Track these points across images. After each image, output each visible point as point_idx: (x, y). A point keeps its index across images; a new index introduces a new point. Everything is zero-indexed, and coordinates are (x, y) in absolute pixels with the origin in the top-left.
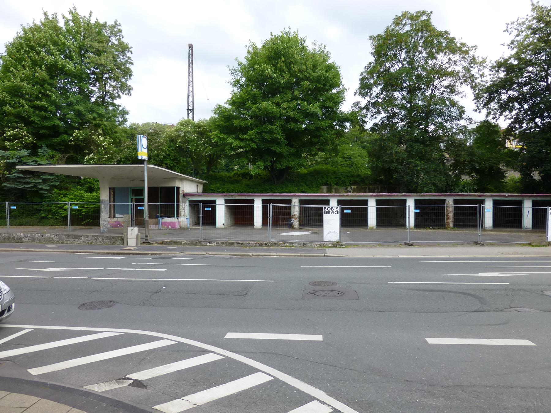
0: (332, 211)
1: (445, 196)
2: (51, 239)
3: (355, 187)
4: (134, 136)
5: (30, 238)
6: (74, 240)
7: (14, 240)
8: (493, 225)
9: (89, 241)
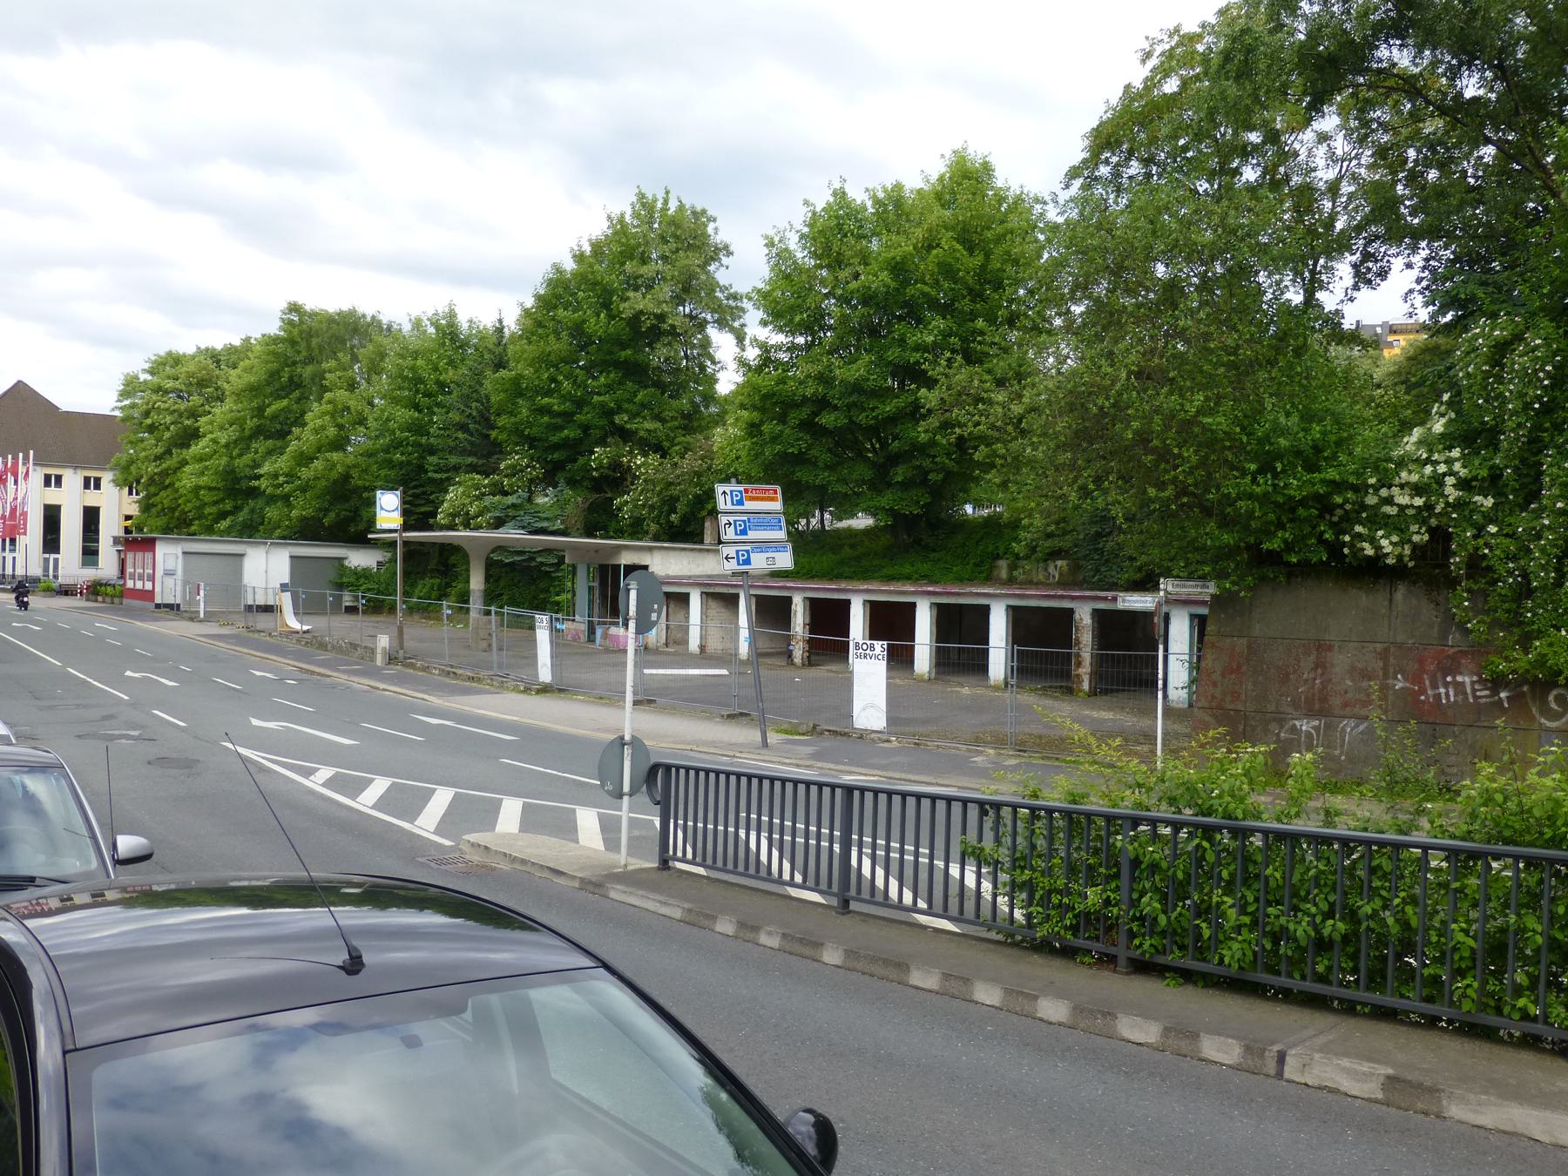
1: (1073, 598)
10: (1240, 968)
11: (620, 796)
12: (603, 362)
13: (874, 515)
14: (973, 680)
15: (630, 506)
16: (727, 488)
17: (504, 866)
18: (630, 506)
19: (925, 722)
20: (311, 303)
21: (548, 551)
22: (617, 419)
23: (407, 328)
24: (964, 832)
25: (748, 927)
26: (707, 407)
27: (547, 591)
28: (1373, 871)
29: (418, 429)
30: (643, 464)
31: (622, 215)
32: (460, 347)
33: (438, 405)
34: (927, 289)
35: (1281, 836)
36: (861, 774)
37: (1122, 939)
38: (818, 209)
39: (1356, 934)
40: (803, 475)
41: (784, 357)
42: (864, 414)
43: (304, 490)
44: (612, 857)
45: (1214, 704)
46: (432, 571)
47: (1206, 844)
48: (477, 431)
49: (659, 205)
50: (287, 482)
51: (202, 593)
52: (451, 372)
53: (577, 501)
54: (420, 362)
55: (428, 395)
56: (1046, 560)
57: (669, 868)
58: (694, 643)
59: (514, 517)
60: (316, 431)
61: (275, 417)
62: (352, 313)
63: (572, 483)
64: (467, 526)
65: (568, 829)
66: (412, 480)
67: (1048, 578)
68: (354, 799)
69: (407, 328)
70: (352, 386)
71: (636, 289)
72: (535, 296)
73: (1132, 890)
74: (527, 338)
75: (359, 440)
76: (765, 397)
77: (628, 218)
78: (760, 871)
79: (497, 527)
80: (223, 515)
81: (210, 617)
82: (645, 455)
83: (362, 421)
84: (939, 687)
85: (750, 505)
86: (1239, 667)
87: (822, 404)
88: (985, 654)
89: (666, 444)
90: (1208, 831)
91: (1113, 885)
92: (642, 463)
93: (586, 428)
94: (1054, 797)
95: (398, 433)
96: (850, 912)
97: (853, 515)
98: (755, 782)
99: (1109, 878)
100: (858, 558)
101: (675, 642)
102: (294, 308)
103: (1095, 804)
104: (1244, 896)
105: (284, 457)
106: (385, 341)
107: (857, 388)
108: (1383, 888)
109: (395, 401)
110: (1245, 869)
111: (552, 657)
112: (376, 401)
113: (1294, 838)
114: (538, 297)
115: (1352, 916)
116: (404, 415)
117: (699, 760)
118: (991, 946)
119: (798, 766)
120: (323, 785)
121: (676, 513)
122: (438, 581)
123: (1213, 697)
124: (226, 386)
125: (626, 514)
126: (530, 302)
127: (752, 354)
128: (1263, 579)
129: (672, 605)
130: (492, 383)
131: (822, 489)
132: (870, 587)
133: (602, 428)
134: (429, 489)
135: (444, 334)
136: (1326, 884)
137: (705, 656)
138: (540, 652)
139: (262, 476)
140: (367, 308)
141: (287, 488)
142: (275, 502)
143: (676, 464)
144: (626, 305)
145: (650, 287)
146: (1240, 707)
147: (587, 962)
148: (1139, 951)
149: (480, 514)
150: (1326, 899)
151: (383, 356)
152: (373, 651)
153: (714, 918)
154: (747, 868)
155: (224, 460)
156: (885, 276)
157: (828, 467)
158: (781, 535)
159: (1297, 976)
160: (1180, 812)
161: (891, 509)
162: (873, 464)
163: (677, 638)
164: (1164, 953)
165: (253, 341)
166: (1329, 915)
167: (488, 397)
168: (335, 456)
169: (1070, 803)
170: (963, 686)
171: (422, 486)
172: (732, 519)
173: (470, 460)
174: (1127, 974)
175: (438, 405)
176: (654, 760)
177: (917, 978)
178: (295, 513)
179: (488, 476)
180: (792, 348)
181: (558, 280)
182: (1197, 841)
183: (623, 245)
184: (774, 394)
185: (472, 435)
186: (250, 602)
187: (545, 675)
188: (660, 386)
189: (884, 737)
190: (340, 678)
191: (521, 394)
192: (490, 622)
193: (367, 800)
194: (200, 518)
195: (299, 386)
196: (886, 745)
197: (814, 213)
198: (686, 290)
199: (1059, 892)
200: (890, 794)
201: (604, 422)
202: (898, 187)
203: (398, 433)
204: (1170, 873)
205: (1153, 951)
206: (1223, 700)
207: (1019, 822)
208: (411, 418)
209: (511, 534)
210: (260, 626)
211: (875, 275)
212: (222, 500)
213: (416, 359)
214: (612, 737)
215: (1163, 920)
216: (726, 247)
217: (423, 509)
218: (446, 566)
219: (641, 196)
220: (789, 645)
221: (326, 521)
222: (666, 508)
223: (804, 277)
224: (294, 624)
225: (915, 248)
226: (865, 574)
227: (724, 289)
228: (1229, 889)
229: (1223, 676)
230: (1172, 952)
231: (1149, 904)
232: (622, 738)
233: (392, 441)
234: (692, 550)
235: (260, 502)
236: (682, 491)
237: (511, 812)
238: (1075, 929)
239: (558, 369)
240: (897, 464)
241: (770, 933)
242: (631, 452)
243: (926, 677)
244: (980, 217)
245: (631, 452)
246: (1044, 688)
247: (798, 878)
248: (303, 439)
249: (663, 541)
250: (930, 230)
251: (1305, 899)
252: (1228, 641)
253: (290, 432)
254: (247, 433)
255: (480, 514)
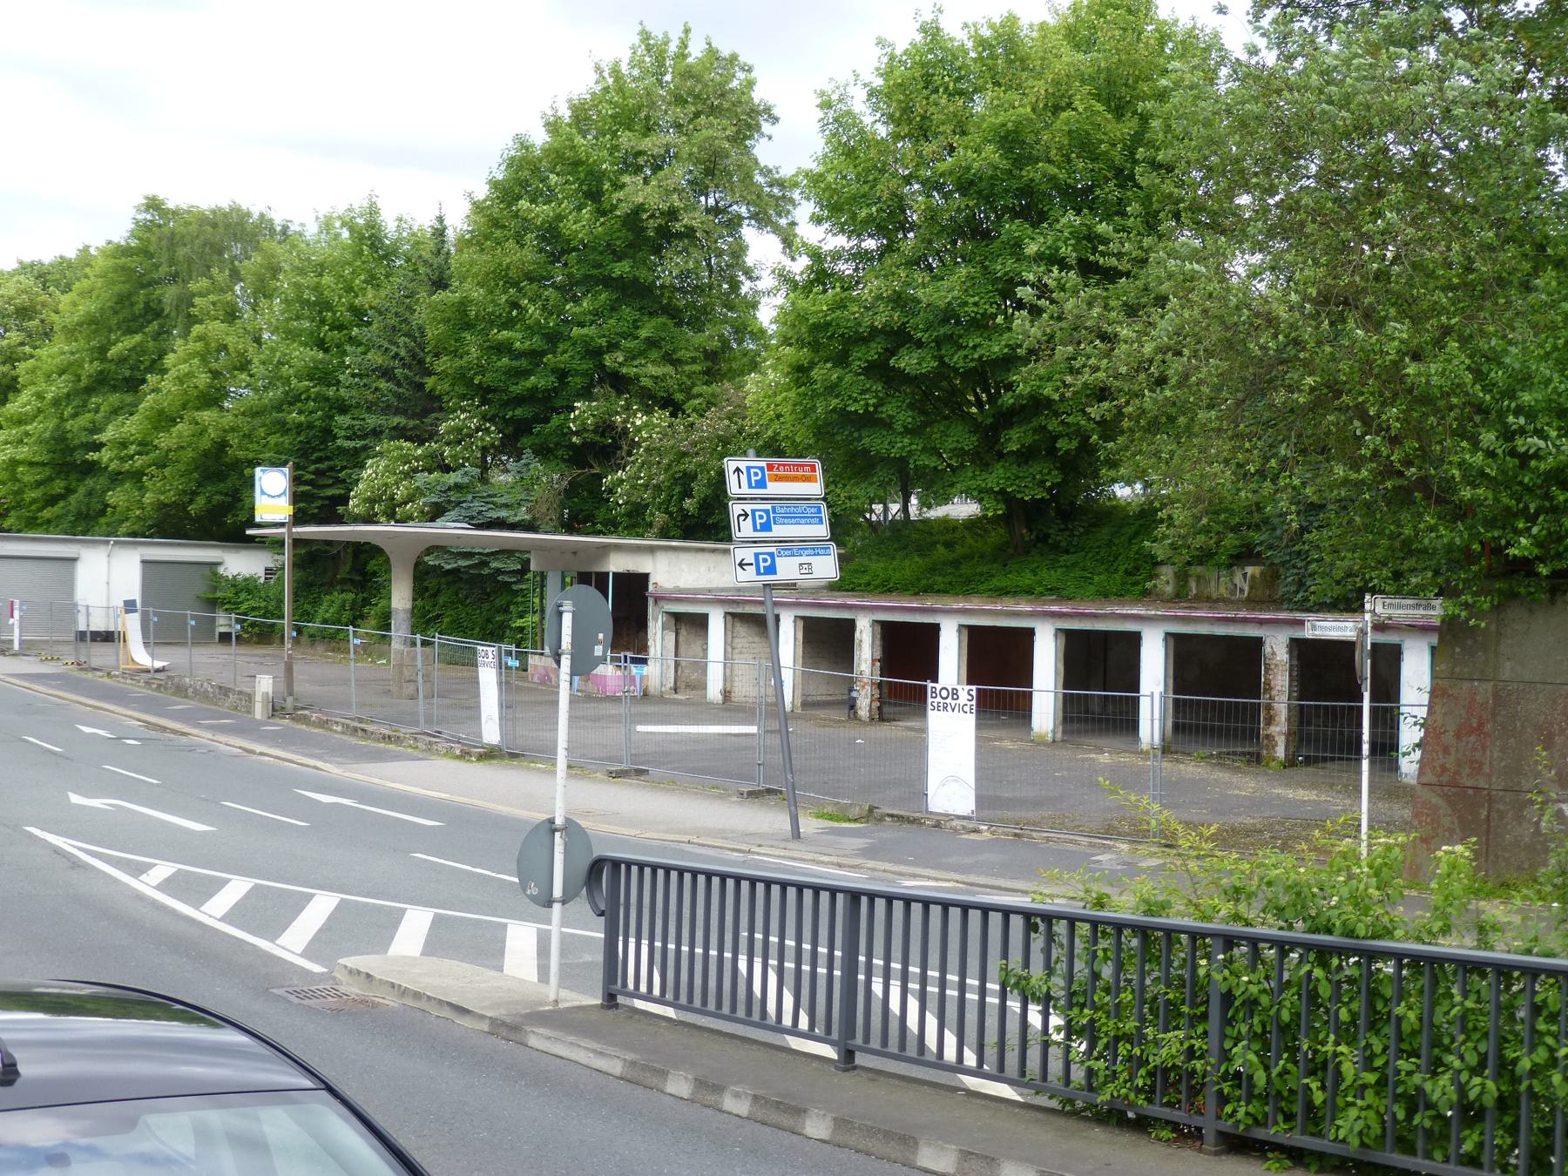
0: (953, 702)
1: (1262, 622)
10: (1363, 1144)
11: (549, 903)
12: (587, 278)
13: (980, 501)
14: (1117, 742)
15: (626, 486)
16: (743, 465)
17: (391, 1001)
18: (626, 486)
19: (1037, 804)
20: (175, 199)
21: (507, 553)
22: (608, 360)
23: (312, 230)
24: (1005, 955)
25: (708, 1087)
26: (740, 342)
27: (506, 610)
28: (1536, 1010)
29: (323, 376)
30: (645, 425)
31: (617, 63)
32: (385, 257)
33: (352, 340)
34: (1052, 170)
35: (1417, 960)
36: (929, 878)
37: (1211, 1104)
38: (898, 52)
39: (1516, 1096)
40: (874, 442)
41: (845, 268)
42: (962, 353)
43: (161, 465)
44: (543, 988)
45: (1445, 779)
46: (343, 581)
47: (1318, 973)
48: (406, 377)
49: (673, 48)
50: (140, 453)
51: (16, 613)
52: (370, 293)
53: (550, 478)
54: (327, 280)
55: (338, 327)
56: (1231, 566)
57: (617, 1006)
58: (714, 690)
59: (458, 504)
60: (180, 380)
61: (122, 360)
62: (236, 209)
63: (543, 452)
64: (391, 515)
65: (490, 950)
66: (314, 450)
67: (1233, 592)
68: (197, 908)
69: (312, 230)
70: (231, 315)
71: (638, 169)
72: (490, 182)
73: (1224, 1036)
74: (479, 244)
75: (241, 393)
76: (816, 328)
77: (624, 68)
78: (754, 1012)
79: (432, 520)
80: (52, 501)
81: (27, 648)
82: (648, 411)
83: (244, 366)
84: (1065, 754)
85: (774, 488)
86: (1481, 725)
87: (899, 338)
88: (1135, 703)
89: (679, 397)
90: (1323, 954)
91: (1200, 1030)
92: (645, 424)
93: (562, 374)
94: (1124, 907)
95: (294, 381)
96: (855, 1068)
97: (946, 500)
98: (955, 913)
99: (1195, 1020)
100: (956, 564)
101: (688, 686)
102: (153, 204)
103: (1180, 917)
104: (1368, 1046)
105: (135, 417)
106: (279, 250)
107: (948, 315)
108: (1549, 1033)
109: (291, 335)
110: (1371, 1005)
111: (501, 706)
112: (266, 336)
113: (1436, 962)
114: (494, 184)
115: (1505, 1068)
116: (304, 355)
117: (794, 871)
118: (1040, 1115)
119: (840, 866)
120: (158, 888)
121: (691, 496)
122: (350, 596)
123: (1444, 769)
124: (55, 317)
125: (620, 497)
126: (482, 192)
127: (800, 266)
128: (1513, 596)
129: (683, 632)
130: (428, 310)
131: (900, 464)
132: (968, 606)
133: (585, 374)
134: (338, 463)
135: (362, 238)
136: (1475, 1029)
137: (729, 707)
138: (484, 700)
139: (102, 445)
140: (254, 204)
141: (139, 461)
142: (122, 482)
143: (692, 425)
144: (621, 194)
145: (657, 168)
146: (1482, 784)
147: (307, 1083)
148: (1230, 1122)
149: (410, 499)
150: (1475, 1048)
151: (275, 271)
152: (250, 698)
153: (663, 1074)
154: (734, 1008)
155: (51, 424)
156: (991, 153)
157: (907, 431)
158: (822, 530)
159: (1438, 1155)
160: (1291, 927)
161: (1002, 492)
162: (975, 426)
163: (689, 680)
164: (1265, 1125)
165: (93, 251)
166: (1477, 1070)
167: (421, 329)
168: (206, 416)
169: (1145, 913)
170: (1102, 752)
171: (328, 458)
172: (748, 508)
173: (396, 420)
174: (1216, 1154)
175: (352, 340)
176: (598, 852)
177: (928, 1157)
178: (149, 498)
179: (421, 443)
180: (861, 256)
181: (523, 158)
182: (1307, 968)
183: (616, 105)
184: (828, 324)
185: (399, 384)
186: (82, 627)
187: (491, 733)
188: (674, 314)
189: (971, 825)
190: (201, 736)
191: (468, 326)
192: (415, 658)
193: (215, 911)
194: (19, 506)
195: (158, 314)
196: (973, 836)
197: (892, 58)
198: (709, 172)
199: (1128, 1038)
200: (965, 908)
201: (587, 365)
202: (1011, 20)
203: (294, 381)
204: (1272, 1012)
205: (1250, 1121)
206: (1457, 773)
207: (1077, 941)
208: (313, 360)
209: (450, 529)
210: (95, 662)
211: (977, 150)
212: (50, 479)
213: (321, 275)
214: (546, 817)
215: (1260, 1077)
216: (768, 110)
217: (330, 492)
218: (363, 573)
219: (646, 36)
220: (851, 690)
221: (192, 509)
222: (678, 489)
223: (873, 153)
224: (143, 658)
225: (1033, 110)
226: (964, 586)
227: (766, 172)
228: (1347, 1034)
229: (1458, 736)
230: (1276, 1123)
231: (1244, 1057)
232: (552, 821)
233: (287, 393)
234: (713, 551)
235: (103, 481)
236: (699, 465)
237: (416, 923)
238: (1150, 1093)
239: (520, 290)
240: (1010, 425)
241: (737, 1095)
242: (627, 408)
243: (1050, 737)
244: (1134, 64)
245: (627, 408)
246: (1219, 755)
247: (970, 1059)
248: (162, 390)
249: (673, 538)
250: (1057, 83)
251: (1448, 1050)
252: (1466, 685)
253: (144, 381)
254: (84, 382)
255: (410, 499)
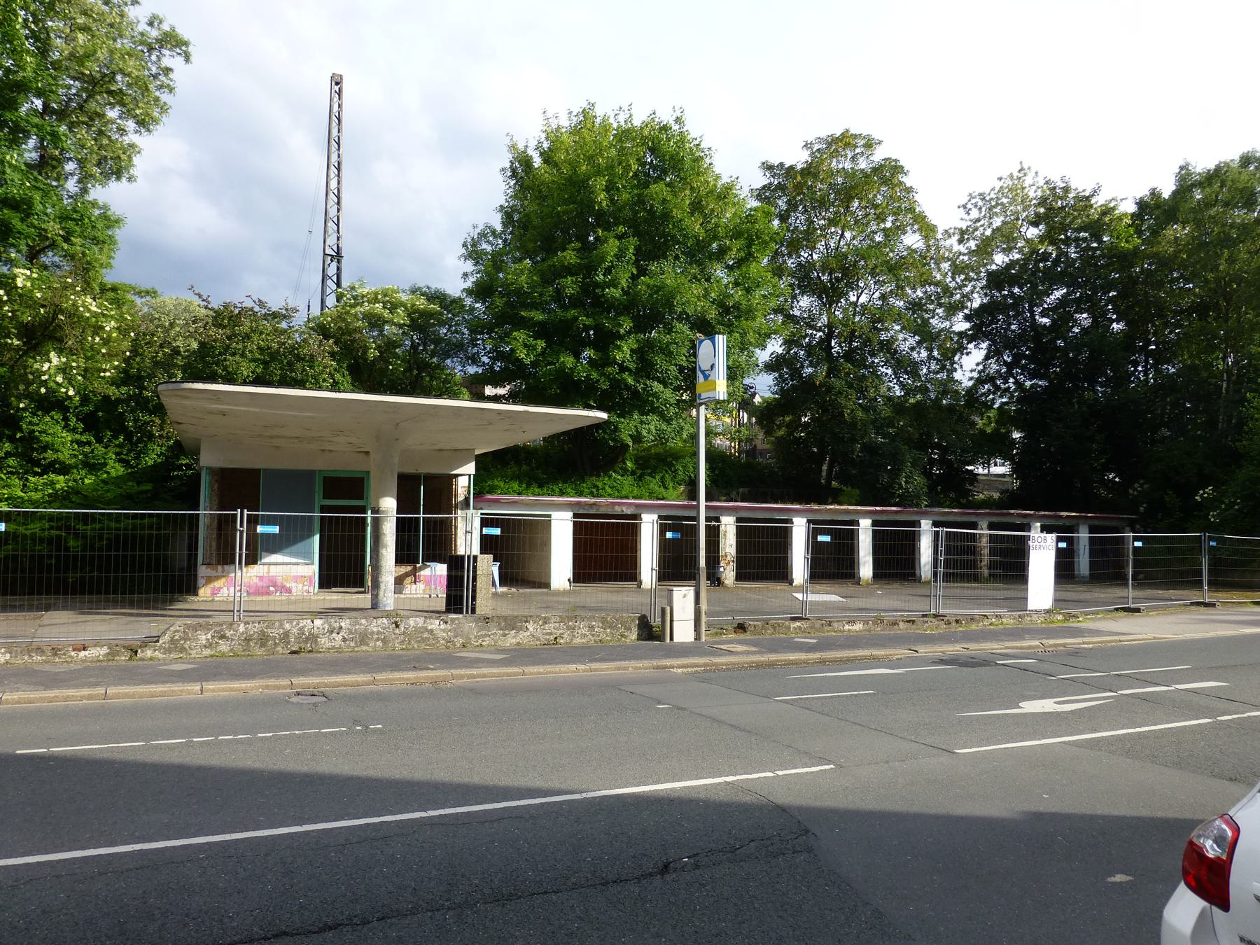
2: (426, 635)
3: (746, 490)
4: (672, 327)
5: (351, 633)
6: (505, 635)
7: (288, 643)
8: (874, 573)
9: (551, 634)
